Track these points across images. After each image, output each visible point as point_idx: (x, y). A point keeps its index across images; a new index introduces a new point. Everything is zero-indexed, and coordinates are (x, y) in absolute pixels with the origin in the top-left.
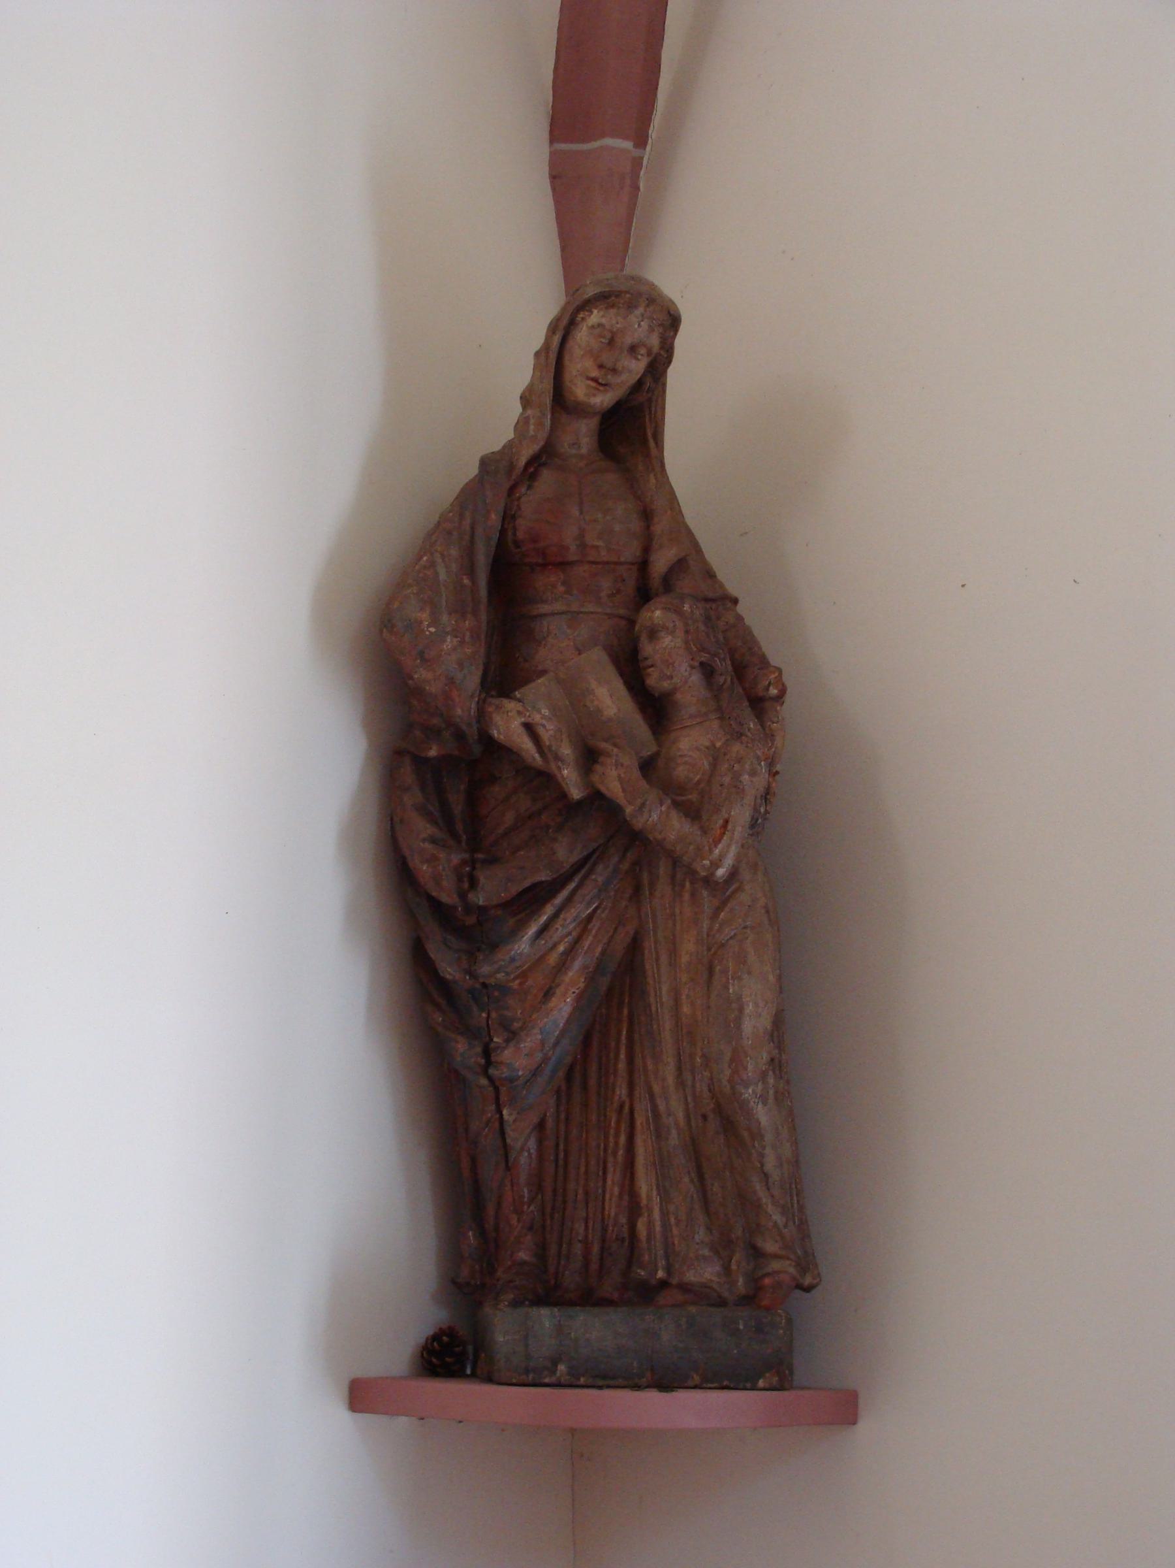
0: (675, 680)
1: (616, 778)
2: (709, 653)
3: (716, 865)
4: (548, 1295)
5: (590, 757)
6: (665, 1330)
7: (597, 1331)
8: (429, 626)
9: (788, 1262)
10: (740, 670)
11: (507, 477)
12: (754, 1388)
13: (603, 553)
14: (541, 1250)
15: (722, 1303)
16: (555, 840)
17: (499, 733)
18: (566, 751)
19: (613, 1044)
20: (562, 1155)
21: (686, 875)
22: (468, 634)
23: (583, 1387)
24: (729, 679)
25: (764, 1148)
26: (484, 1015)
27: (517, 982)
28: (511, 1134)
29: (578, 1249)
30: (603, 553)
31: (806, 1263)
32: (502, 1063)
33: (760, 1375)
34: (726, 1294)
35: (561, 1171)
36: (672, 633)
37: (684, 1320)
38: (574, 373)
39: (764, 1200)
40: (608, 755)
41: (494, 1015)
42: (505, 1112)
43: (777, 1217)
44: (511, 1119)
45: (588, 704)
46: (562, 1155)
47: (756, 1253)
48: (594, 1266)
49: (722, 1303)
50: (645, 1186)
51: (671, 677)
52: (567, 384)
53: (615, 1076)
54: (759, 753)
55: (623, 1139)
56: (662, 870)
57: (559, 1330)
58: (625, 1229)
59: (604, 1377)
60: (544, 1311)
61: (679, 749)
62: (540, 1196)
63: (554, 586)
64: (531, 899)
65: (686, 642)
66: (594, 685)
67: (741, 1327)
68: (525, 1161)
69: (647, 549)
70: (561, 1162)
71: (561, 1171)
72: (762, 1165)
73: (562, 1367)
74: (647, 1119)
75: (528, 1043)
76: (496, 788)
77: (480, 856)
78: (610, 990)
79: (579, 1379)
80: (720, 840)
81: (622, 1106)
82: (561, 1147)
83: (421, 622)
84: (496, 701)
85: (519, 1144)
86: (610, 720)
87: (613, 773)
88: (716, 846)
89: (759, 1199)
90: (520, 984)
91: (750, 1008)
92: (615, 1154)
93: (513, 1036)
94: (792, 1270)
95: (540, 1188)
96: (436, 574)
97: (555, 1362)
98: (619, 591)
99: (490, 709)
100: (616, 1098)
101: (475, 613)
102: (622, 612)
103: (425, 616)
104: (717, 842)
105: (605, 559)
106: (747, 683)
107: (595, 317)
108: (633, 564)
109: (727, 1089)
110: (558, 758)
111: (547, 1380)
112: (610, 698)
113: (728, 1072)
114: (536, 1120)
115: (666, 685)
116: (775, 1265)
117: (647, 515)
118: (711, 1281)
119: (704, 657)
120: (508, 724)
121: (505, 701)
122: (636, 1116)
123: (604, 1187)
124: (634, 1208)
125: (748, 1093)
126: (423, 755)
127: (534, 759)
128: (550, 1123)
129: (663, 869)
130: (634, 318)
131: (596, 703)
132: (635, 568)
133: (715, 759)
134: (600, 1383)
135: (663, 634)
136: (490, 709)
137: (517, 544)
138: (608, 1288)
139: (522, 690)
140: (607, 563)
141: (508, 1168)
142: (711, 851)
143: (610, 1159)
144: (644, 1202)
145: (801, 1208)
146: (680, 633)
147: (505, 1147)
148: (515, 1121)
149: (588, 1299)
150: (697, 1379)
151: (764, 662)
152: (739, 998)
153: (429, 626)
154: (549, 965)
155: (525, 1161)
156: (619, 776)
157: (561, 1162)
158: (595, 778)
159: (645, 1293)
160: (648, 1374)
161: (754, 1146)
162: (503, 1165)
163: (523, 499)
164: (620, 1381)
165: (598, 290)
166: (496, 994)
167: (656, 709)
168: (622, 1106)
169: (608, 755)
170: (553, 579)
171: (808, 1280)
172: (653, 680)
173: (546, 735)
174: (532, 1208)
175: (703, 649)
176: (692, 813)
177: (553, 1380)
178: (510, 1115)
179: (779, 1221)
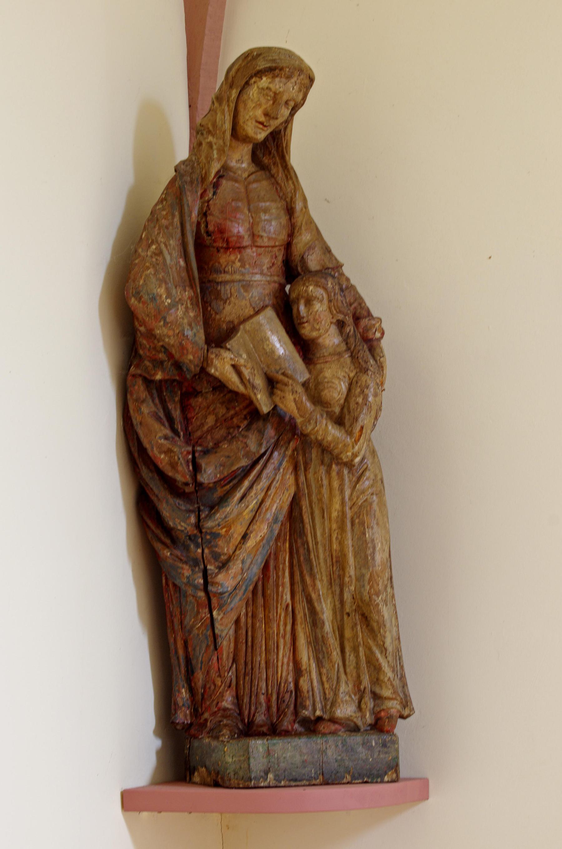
0: (321, 331)
1: (292, 402)
2: (343, 314)
3: (355, 455)
4: (249, 730)
5: (272, 383)
6: (329, 749)
7: (292, 751)
8: (166, 298)
9: (395, 702)
10: (357, 319)
12: (382, 782)
13: (266, 240)
14: (238, 697)
15: (356, 729)
16: (246, 437)
17: (216, 370)
18: (259, 382)
19: (281, 566)
20: (250, 639)
21: (329, 455)
22: (189, 302)
23: (284, 787)
24: (352, 329)
25: (385, 632)
26: (200, 551)
27: (224, 530)
28: (217, 625)
29: (262, 698)
30: (266, 240)
31: (406, 702)
32: (217, 583)
33: (386, 773)
34: (360, 723)
35: (250, 650)
36: (321, 301)
37: (340, 742)
38: (247, 117)
39: (383, 664)
41: (206, 551)
42: (215, 613)
43: (390, 674)
44: (220, 618)
45: (265, 347)
46: (250, 639)
47: (376, 696)
48: (274, 709)
49: (356, 729)
50: (305, 655)
51: (319, 330)
52: (241, 122)
53: (283, 587)
54: (378, 381)
55: (289, 628)
56: (314, 456)
57: (268, 753)
58: (292, 686)
59: (296, 780)
61: (325, 378)
62: (234, 666)
63: (234, 262)
64: (235, 479)
65: (330, 308)
66: (269, 333)
67: (374, 744)
68: (226, 645)
69: (291, 235)
70: (250, 644)
71: (250, 650)
72: (384, 643)
73: (271, 776)
74: (305, 615)
75: (235, 568)
76: (200, 399)
77: (199, 448)
78: (279, 535)
79: (281, 783)
80: (359, 440)
81: (287, 606)
82: (250, 633)
83: (161, 296)
84: (214, 350)
85: (224, 634)
86: (279, 357)
87: (290, 397)
88: (356, 444)
89: (380, 664)
90: (226, 531)
91: (379, 546)
92: (284, 637)
93: (224, 566)
94: (399, 707)
95: (235, 660)
96: (164, 259)
97: (266, 773)
98: (273, 264)
99: (213, 356)
100: (284, 601)
101: (192, 286)
102: (276, 278)
103: (162, 291)
104: (356, 442)
105: (266, 244)
106: (362, 334)
107: (264, 82)
108: (282, 246)
109: (367, 598)
110: (253, 387)
111: (262, 784)
112: (279, 344)
113: (368, 588)
114: (235, 618)
115: (315, 334)
116: (390, 704)
117: (290, 211)
118: (351, 716)
119: (341, 317)
120: (222, 366)
121: (222, 351)
122: (297, 612)
123: (277, 658)
124: (298, 671)
125: (379, 600)
126: (153, 378)
127: (238, 387)
128: (243, 619)
129: (314, 454)
130: (290, 85)
131: (270, 346)
132: (282, 248)
133: (350, 384)
134: (293, 783)
135: (315, 302)
136: (213, 356)
137: (208, 233)
138: (286, 724)
139: (230, 342)
140: (268, 247)
141: (216, 649)
142: (353, 447)
143: (282, 641)
144: (304, 667)
145: (402, 667)
146: (326, 301)
147: (215, 637)
148: (221, 619)
149: (274, 731)
150: (349, 778)
151: (369, 314)
152: (373, 540)
153: (166, 298)
154: (249, 524)
155: (226, 645)
156: (295, 399)
157: (250, 644)
158: (277, 400)
159: (311, 726)
160: (321, 777)
161: (380, 632)
162: (212, 647)
163: (211, 202)
164: (304, 782)
165: (268, 65)
166: (208, 537)
167: (305, 348)
168: (287, 606)
169: (286, 385)
170: (233, 257)
171: (406, 713)
172: (307, 331)
173: (246, 372)
174: (230, 674)
175: (340, 312)
176: (339, 421)
177: (266, 784)
178: (219, 614)
179: (391, 676)
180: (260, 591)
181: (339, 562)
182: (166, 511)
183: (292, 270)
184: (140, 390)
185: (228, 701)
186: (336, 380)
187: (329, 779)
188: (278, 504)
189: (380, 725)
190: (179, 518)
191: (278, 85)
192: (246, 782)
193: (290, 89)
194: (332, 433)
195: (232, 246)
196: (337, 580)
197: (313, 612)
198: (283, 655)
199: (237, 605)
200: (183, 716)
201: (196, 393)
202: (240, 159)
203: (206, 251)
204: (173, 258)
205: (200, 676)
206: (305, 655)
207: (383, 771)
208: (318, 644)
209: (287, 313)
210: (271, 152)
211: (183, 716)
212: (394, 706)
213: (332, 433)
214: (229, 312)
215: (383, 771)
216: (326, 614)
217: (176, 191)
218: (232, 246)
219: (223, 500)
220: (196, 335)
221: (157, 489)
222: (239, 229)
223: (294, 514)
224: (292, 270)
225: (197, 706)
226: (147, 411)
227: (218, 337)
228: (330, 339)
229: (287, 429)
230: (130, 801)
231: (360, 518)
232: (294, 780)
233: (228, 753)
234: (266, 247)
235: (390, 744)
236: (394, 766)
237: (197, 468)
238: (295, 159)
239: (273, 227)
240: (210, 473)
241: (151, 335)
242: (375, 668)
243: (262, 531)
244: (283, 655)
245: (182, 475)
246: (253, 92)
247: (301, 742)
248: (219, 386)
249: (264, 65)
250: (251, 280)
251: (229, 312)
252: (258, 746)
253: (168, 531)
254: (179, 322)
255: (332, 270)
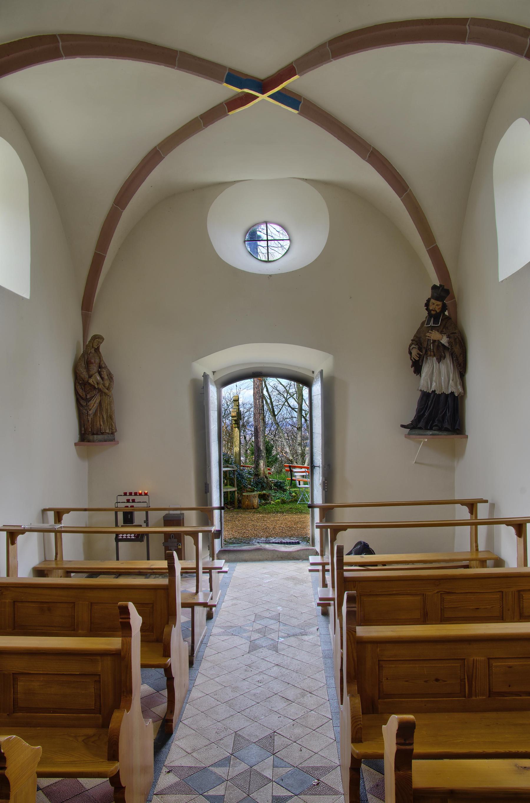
1: (101, 386)
4: (93, 434)
5: (98, 384)
6: (106, 437)
7: (100, 437)
11: (85, 353)
21: (106, 394)
31: (116, 430)
40: (356, 603)
50: (101, 423)
60: (251, 392)
68: (90, 422)
75: (92, 410)
93: (90, 410)
106: (110, 377)
112: (99, 378)
117: (100, 358)
120: (91, 381)
149: (97, 434)
154: (94, 404)
155: (90, 422)
159: (102, 434)
167: (102, 378)
172: (102, 376)
176: (107, 389)
180: (95, 414)
181: (107, 410)
182: (81, 402)
183: (100, 367)
184: (77, 384)
185: (90, 430)
186: (107, 383)
187: (106, 441)
188: (98, 401)
189: (113, 433)
190: (83, 403)
191: (99, 340)
192: (94, 441)
193: (101, 341)
194: (106, 391)
195: (92, 363)
196: (107, 412)
197: (103, 417)
198: (98, 423)
199: (92, 416)
200: (83, 432)
201: (86, 385)
202: (93, 351)
203: (88, 363)
204: (83, 365)
205: (86, 426)
206: (101, 423)
207: (113, 440)
208: (104, 422)
209: (100, 373)
210: (97, 350)
211: (83, 432)
212: (114, 430)
213: (106, 391)
214: (91, 373)
215: (113, 440)
216: (105, 417)
217: (83, 355)
218: (92, 363)
219: (90, 400)
220: (87, 376)
221: (80, 398)
222: (93, 361)
223: (100, 403)
224: (100, 367)
225: (85, 430)
226: (79, 387)
227: (90, 377)
228: (106, 377)
229: (100, 390)
230: (76, 444)
231: (110, 403)
232: (100, 441)
233: (91, 437)
234: (240, 449)
235: (114, 436)
236: (114, 439)
237: (86, 396)
238: (101, 350)
239: (97, 361)
240: (88, 397)
241: (80, 376)
242: (112, 425)
243: (96, 405)
244: (98, 423)
245: (84, 397)
246: (95, 341)
247: (102, 436)
248: (90, 384)
249: (98, 338)
250: (94, 368)
251: (91, 373)
252: (95, 436)
253: (81, 405)
254: (84, 374)
255: (106, 367)
